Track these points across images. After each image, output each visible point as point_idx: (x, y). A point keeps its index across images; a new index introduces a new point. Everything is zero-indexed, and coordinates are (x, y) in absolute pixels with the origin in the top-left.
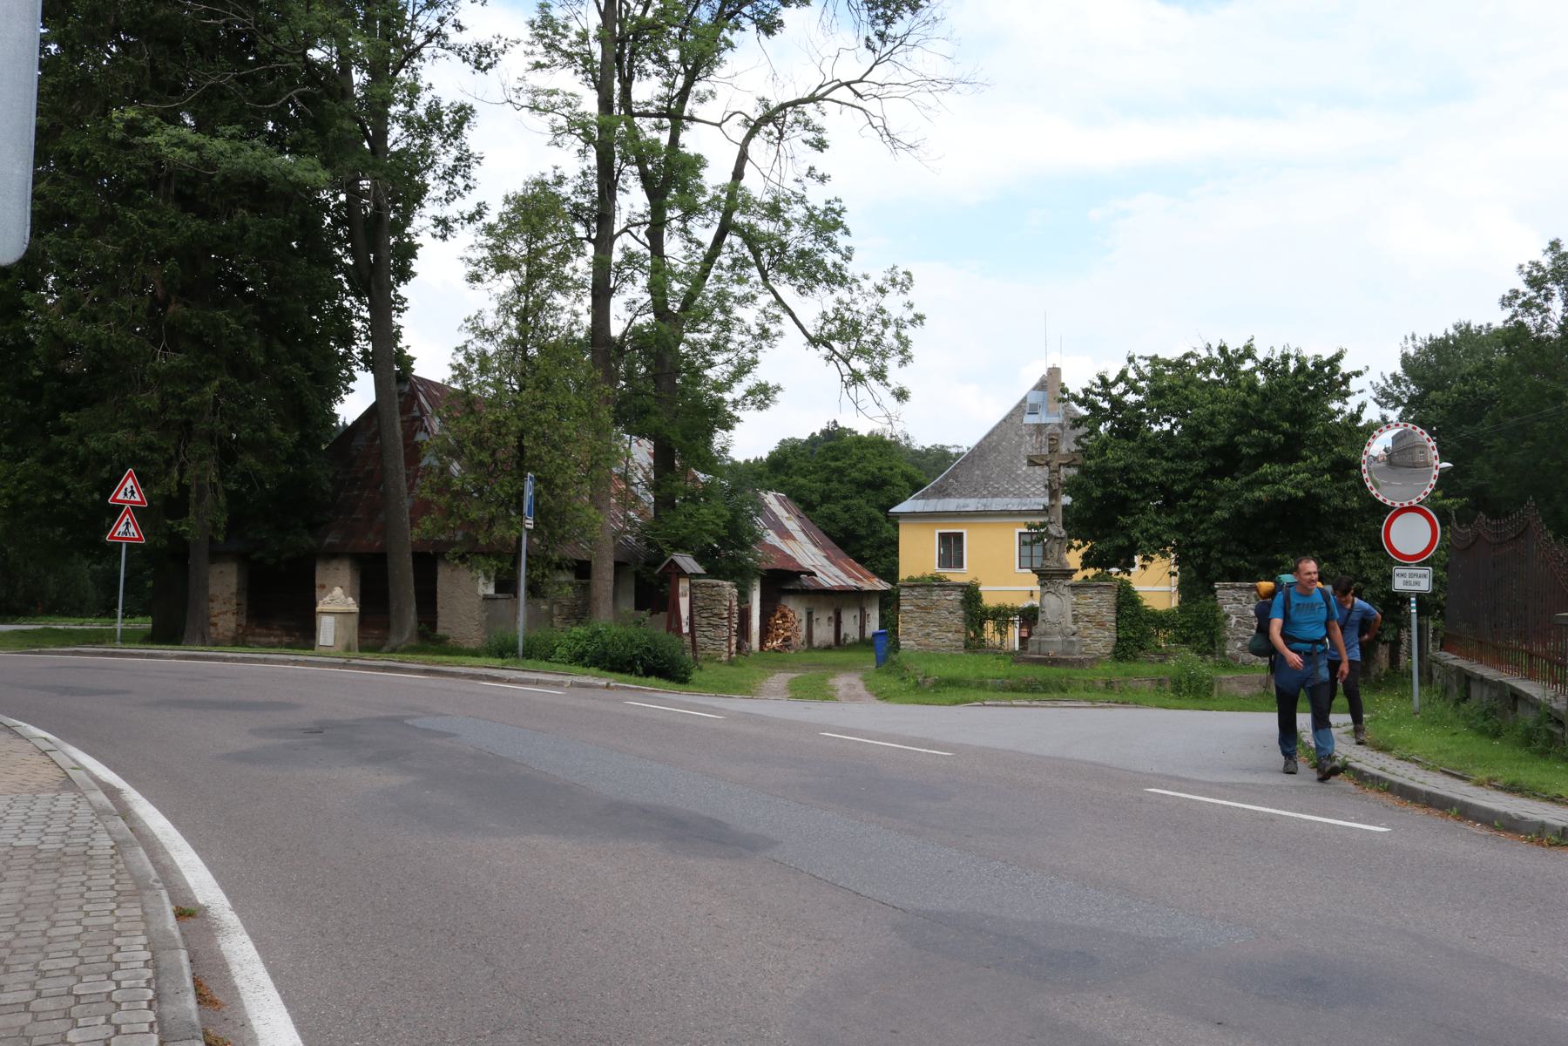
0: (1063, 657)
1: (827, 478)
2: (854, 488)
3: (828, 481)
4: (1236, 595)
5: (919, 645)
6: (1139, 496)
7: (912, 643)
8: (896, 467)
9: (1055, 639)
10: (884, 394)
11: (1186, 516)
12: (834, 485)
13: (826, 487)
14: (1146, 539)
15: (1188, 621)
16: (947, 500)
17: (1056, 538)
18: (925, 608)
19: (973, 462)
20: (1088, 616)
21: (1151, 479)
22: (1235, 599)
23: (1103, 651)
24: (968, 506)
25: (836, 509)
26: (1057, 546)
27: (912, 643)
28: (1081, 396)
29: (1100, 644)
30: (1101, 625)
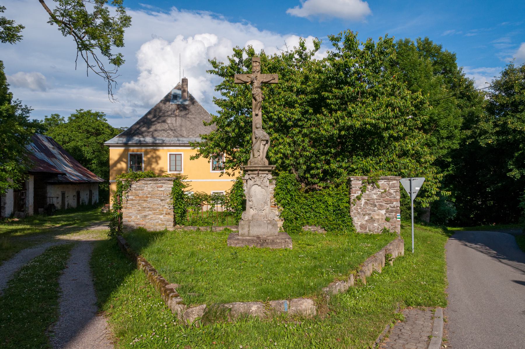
10: (104, 60)
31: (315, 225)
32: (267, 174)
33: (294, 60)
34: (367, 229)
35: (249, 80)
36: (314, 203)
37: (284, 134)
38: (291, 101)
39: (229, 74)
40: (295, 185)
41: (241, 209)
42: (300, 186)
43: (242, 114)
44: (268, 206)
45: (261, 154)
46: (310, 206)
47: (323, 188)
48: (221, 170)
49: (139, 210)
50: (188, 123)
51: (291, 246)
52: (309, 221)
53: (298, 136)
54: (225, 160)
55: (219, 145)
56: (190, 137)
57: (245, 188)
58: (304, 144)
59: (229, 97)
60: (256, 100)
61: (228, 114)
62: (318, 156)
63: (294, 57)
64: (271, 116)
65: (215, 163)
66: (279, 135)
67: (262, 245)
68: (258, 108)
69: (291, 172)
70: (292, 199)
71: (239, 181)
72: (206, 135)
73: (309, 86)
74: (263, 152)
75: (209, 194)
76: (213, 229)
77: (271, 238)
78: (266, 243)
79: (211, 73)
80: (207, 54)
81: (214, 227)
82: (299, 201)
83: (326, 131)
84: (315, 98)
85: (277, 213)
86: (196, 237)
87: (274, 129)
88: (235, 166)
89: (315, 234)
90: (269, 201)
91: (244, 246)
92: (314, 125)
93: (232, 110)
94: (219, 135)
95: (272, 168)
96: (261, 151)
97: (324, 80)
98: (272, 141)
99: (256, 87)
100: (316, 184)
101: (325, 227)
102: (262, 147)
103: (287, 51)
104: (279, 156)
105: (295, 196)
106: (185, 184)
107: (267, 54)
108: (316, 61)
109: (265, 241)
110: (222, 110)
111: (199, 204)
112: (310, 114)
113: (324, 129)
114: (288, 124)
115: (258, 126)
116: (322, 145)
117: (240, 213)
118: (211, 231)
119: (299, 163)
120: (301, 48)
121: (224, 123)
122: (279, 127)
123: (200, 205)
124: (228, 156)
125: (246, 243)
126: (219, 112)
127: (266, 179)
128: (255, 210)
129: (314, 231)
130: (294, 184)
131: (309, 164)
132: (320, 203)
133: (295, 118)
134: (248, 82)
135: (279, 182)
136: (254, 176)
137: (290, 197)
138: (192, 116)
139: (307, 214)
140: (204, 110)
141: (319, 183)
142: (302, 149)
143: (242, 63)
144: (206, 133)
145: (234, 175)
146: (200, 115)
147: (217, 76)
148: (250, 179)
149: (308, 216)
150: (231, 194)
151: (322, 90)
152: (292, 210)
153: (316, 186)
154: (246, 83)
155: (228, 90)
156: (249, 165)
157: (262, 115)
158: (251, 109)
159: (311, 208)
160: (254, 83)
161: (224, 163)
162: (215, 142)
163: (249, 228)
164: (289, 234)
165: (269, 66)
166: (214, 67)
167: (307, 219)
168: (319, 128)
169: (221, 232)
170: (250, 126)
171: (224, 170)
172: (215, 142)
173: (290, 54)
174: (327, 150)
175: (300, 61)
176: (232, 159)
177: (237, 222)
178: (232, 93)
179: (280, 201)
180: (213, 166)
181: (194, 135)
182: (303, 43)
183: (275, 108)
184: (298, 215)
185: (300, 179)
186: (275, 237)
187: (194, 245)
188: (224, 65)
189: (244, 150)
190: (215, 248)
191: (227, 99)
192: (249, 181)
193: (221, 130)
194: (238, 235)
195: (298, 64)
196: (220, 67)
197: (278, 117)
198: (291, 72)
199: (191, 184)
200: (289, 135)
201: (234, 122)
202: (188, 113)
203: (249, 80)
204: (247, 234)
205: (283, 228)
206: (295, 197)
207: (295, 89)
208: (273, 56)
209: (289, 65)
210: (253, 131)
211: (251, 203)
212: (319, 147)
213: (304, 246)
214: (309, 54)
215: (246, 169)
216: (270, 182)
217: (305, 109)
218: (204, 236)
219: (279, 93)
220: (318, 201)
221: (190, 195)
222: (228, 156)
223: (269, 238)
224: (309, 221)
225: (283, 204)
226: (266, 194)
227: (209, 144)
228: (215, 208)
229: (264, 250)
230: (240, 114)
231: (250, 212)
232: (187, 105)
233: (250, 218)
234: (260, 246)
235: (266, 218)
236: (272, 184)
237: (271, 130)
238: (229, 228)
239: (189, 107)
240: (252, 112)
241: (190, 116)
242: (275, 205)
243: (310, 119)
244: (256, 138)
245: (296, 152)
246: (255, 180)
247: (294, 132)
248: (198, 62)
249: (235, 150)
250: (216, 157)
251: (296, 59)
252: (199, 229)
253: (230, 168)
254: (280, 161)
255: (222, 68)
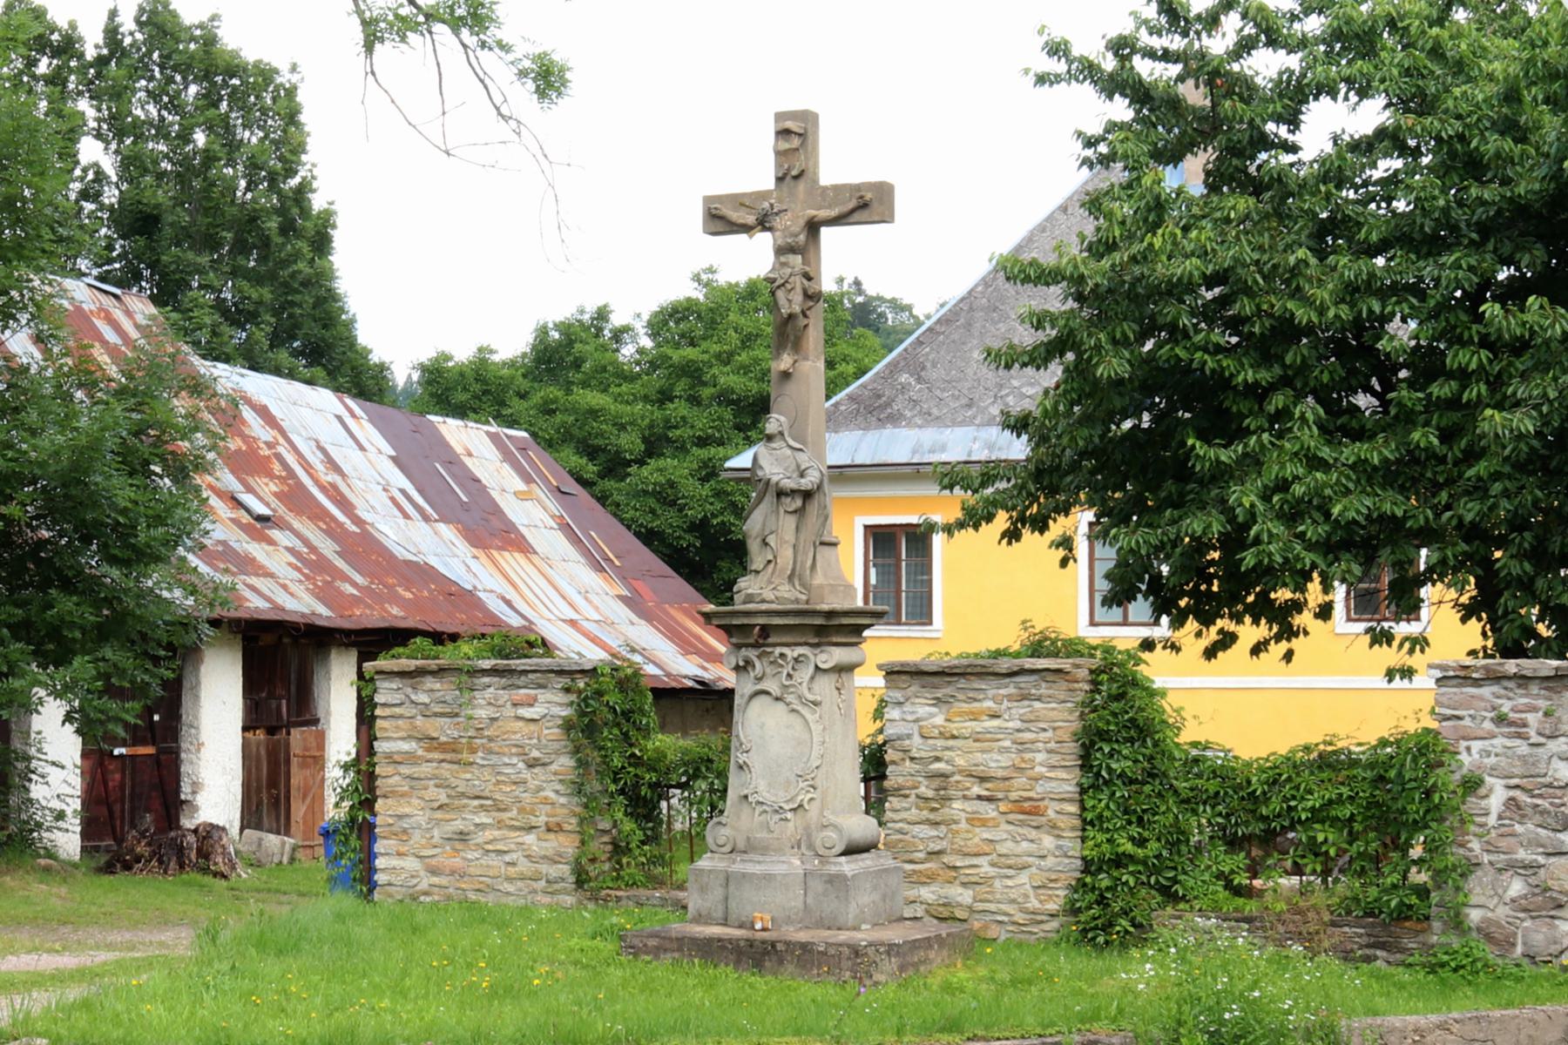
0: (803, 937)
1: (661, 392)
2: (728, 414)
3: (665, 397)
4: (1506, 706)
5: (434, 871)
6: (1264, 376)
7: (411, 864)
8: (845, 359)
9: (779, 869)
11: (1416, 436)
12: (678, 409)
13: (658, 414)
14: (1280, 516)
15: (1340, 800)
16: (888, 431)
17: (781, 493)
18: (451, 747)
19: (968, 325)
20: (983, 779)
21: (1302, 315)
22: (1501, 720)
23: (1034, 904)
24: (943, 448)
25: (669, 468)
26: (789, 523)
27: (411, 864)
28: (1109, 64)
29: (1023, 878)
30: (1029, 810)
34: (1519, 949)
49: (440, 807)
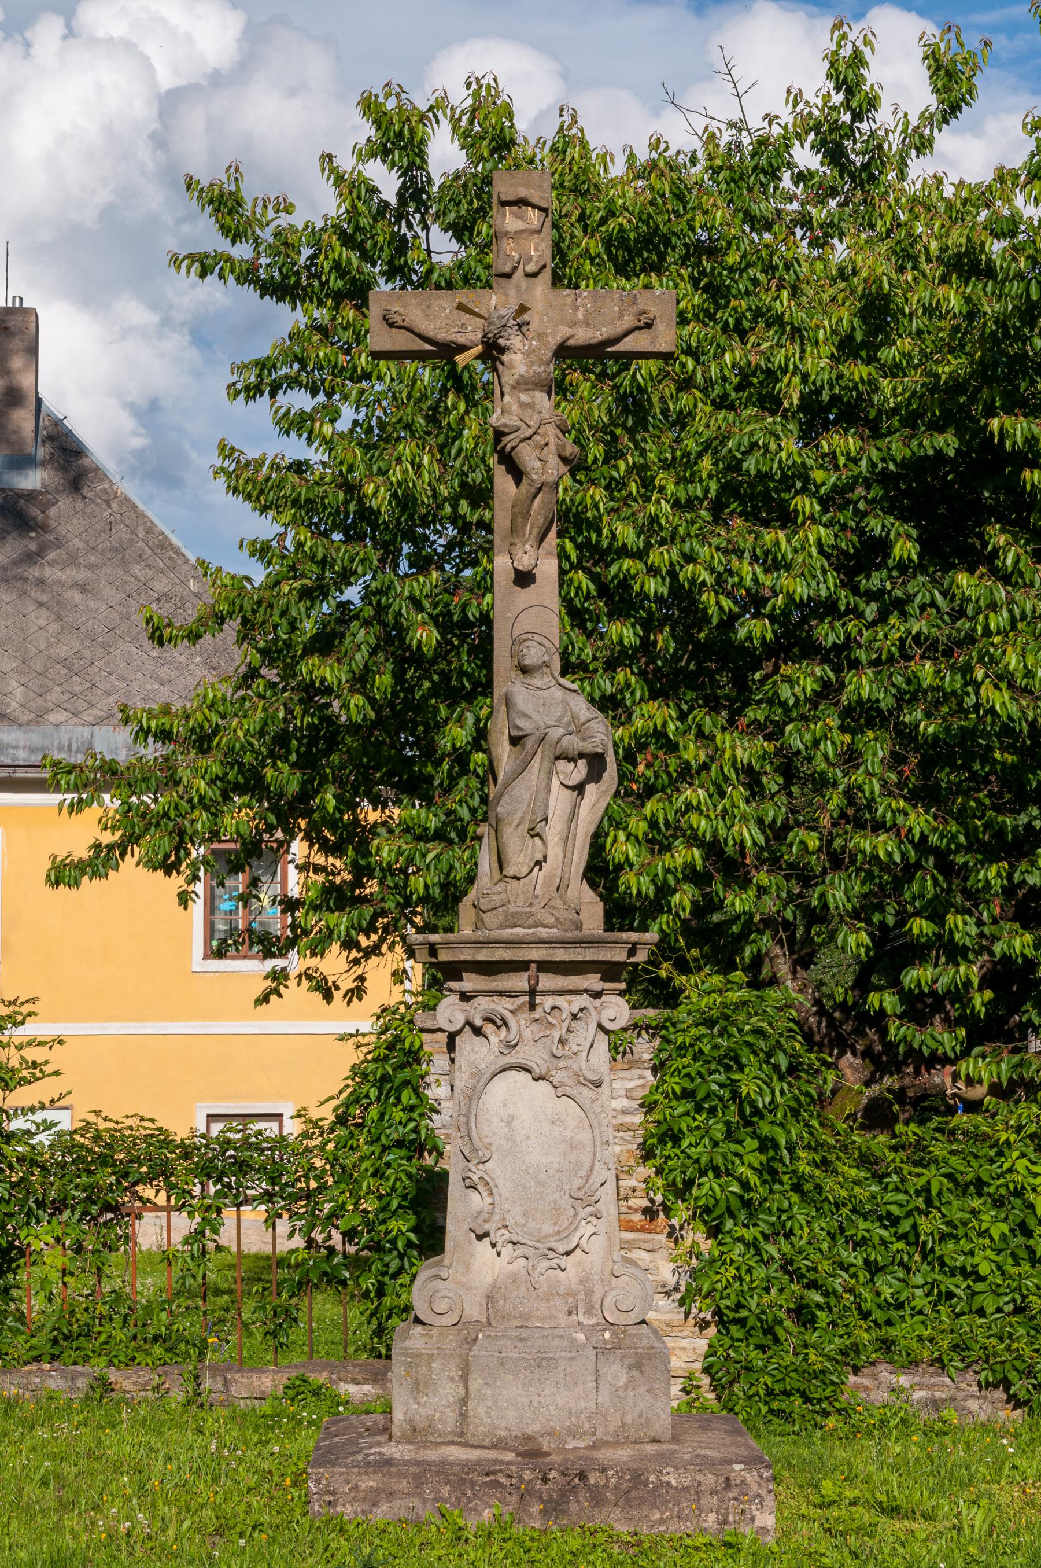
31: (940, 1363)
32: (597, 995)
33: (786, 181)
35: (472, 333)
36: (929, 1202)
37: (713, 705)
38: (767, 476)
39: (336, 283)
40: (793, 1069)
41: (410, 1244)
42: (831, 1076)
43: (422, 564)
44: (601, 1225)
45: (554, 850)
46: (905, 1226)
47: (996, 1090)
48: (268, 954)
50: (39, 618)
51: (766, 1519)
52: (893, 1332)
53: (816, 719)
54: (294, 884)
55: (260, 778)
56: (54, 717)
57: (436, 1091)
58: (859, 777)
59: (329, 444)
60: (517, 474)
61: (323, 563)
62: (960, 860)
63: (790, 165)
64: (625, 583)
65: (226, 906)
66: (682, 717)
67: (554, 1507)
68: (531, 530)
69: (766, 972)
70: (769, 1173)
71: (398, 1039)
72: (166, 710)
73: (894, 370)
74: (566, 840)
75: (180, 1134)
76: (207, 1383)
77: (623, 1454)
78: (583, 1493)
79: (203, 275)
80: (159, 141)
81: (214, 1369)
82: (819, 1188)
83: (1011, 686)
84: (939, 452)
85: (666, 1272)
86: (82, 1449)
87: (642, 674)
88: (368, 930)
89: (942, 1431)
90: (611, 1186)
91: (427, 1513)
92: (930, 648)
93: (353, 536)
94: (260, 714)
95: (632, 952)
96: (553, 831)
97: (1001, 322)
98: (629, 757)
99: (518, 386)
100: (946, 1060)
101: (1013, 1376)
102: (559, 800)
103: (736, 116)
104: (680, 860)
105: (791, 1148)
106: (14, 1063)
107: (596, 140)
108: (949, 191)
109: (582, 1476)
110: (281, 537)
111: (107, 1208)
112: (903, 567)
113: (1004, 678)
114: (742, 633)
115: (533, 655)
116: (987, 782)
117: (401, 1270)
118: (195, 1400)
119: (825, 906)
120: (838, 98)
121: (293, 626)
122: (676, 657)
123: (114, 1208)
124: (319, 859)
125: (445, 1491)
126: (261, 551)
127: (586, 1031)
128: (507, 1251)
129: (935, 1404)
130: (783, 1062)
131: (890, 920)
132: (976, 1203)
133: (790, 596)
134: (462, 348)
135: (682, 1047)
136: (502, 1006)
137: (756, 1159)
138: (69, 575)
139: (879, 1281)
140: (150, 529)
141: (966, 1053)
142: (843, 815)
143: (422, 207)
144: (164, 695)
145: (357, 992)
146: (124, 563)
147: (250, 293)
148: (478, 1031)
149: (887, 1292)
150: (341, 1132)
151: (985, 394)
152: (772, 1250)
153: (941, 1078)
154: (447, 351)
155: (321, 398)
156: (466, 931)
157: (562, 572)
158: (489, 528)
159: (912, 1238)
160: (503, 350)
161: (290, 905)
162: (232, 758)
163: (465, 1378)
164: (753, 1429)
165: (612, 224)
166: (225, 230)
167: (878, 1315)
168: (967, 670)
169: (266, 1407)
170: (473, 651)
171: (293, 954)
172: (232, 758)
173: (763, 142)
174: (1023, 819)
175: (833, 192)
176: (347, 877)
177: (380, 1332)
178: (348, 414)
179: (689, 1184)
180: (210, 930)
181: (81, 704)
182: (857, 60)
183: (654, 519)
184: (813, 1285)
185: (832, 1024)
186: (651, 1449)
187: (65, 1506)
188: (298, 220)
189: (433, 823)
190: (219, 1531)
191: (315, 455)
192: (466, 1042)
193: (270, 674)
194: (386, 1430)
195: (818, 214)
196: (267, 235)
197: (676, 588)
198: (770, 268)
199: (56, 1058)
200: (751, 713)
201: (367, 623)
202: (40, 553)
203: (472, 333)
204: (448, 1422)
205: (706, 1381)
206: (794, 1158)
207: (793, 392)
208: (643, 155)
209: (749, 218)
210: (499, 690)
211: (477, 1201)
212: (966, 794)
213: (864, 1515)
214: (895, 141)
215: (444, 956)
216: (614, 1048)
217: (861, 532)
218: (141, 1436)
219: (683, 420)
220: (962, 1189)
221: (44, 1139)
222: (319, 859)
223: (604, 1455)
224: (893, 1332)
225: (707, 1210)
226: (585, 1136)
227: (184, 774)
228: (227, 1236)
229: (575, 1544)
230: (404, 567)
231: (476, 1267)
232: (31, 496)
233: (474, 1312)
234: (544, 1512)
235: (589, 1312)
236: (632, 1065)
237: (620, 676)
238: (318, 1378)
239: (44, 508)
240: (488, 549)
241: (49, 573)
242: (650, 1212)
243: (900, 606)
244: (515, 741)
245: (801, 834)
246: (513, 1035)
247: (785, 692)
248: (104, 196)
249: (371, 815)
250: (236, 868)
251: (801, 177)
252: (107, 1387)
253: (336, 947)
254: (684, 898)
255: (284, 242)
